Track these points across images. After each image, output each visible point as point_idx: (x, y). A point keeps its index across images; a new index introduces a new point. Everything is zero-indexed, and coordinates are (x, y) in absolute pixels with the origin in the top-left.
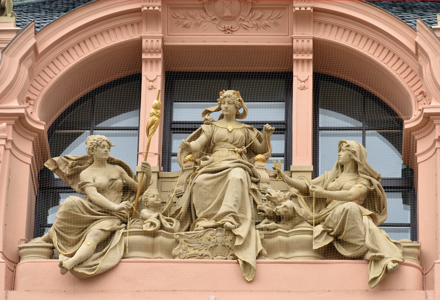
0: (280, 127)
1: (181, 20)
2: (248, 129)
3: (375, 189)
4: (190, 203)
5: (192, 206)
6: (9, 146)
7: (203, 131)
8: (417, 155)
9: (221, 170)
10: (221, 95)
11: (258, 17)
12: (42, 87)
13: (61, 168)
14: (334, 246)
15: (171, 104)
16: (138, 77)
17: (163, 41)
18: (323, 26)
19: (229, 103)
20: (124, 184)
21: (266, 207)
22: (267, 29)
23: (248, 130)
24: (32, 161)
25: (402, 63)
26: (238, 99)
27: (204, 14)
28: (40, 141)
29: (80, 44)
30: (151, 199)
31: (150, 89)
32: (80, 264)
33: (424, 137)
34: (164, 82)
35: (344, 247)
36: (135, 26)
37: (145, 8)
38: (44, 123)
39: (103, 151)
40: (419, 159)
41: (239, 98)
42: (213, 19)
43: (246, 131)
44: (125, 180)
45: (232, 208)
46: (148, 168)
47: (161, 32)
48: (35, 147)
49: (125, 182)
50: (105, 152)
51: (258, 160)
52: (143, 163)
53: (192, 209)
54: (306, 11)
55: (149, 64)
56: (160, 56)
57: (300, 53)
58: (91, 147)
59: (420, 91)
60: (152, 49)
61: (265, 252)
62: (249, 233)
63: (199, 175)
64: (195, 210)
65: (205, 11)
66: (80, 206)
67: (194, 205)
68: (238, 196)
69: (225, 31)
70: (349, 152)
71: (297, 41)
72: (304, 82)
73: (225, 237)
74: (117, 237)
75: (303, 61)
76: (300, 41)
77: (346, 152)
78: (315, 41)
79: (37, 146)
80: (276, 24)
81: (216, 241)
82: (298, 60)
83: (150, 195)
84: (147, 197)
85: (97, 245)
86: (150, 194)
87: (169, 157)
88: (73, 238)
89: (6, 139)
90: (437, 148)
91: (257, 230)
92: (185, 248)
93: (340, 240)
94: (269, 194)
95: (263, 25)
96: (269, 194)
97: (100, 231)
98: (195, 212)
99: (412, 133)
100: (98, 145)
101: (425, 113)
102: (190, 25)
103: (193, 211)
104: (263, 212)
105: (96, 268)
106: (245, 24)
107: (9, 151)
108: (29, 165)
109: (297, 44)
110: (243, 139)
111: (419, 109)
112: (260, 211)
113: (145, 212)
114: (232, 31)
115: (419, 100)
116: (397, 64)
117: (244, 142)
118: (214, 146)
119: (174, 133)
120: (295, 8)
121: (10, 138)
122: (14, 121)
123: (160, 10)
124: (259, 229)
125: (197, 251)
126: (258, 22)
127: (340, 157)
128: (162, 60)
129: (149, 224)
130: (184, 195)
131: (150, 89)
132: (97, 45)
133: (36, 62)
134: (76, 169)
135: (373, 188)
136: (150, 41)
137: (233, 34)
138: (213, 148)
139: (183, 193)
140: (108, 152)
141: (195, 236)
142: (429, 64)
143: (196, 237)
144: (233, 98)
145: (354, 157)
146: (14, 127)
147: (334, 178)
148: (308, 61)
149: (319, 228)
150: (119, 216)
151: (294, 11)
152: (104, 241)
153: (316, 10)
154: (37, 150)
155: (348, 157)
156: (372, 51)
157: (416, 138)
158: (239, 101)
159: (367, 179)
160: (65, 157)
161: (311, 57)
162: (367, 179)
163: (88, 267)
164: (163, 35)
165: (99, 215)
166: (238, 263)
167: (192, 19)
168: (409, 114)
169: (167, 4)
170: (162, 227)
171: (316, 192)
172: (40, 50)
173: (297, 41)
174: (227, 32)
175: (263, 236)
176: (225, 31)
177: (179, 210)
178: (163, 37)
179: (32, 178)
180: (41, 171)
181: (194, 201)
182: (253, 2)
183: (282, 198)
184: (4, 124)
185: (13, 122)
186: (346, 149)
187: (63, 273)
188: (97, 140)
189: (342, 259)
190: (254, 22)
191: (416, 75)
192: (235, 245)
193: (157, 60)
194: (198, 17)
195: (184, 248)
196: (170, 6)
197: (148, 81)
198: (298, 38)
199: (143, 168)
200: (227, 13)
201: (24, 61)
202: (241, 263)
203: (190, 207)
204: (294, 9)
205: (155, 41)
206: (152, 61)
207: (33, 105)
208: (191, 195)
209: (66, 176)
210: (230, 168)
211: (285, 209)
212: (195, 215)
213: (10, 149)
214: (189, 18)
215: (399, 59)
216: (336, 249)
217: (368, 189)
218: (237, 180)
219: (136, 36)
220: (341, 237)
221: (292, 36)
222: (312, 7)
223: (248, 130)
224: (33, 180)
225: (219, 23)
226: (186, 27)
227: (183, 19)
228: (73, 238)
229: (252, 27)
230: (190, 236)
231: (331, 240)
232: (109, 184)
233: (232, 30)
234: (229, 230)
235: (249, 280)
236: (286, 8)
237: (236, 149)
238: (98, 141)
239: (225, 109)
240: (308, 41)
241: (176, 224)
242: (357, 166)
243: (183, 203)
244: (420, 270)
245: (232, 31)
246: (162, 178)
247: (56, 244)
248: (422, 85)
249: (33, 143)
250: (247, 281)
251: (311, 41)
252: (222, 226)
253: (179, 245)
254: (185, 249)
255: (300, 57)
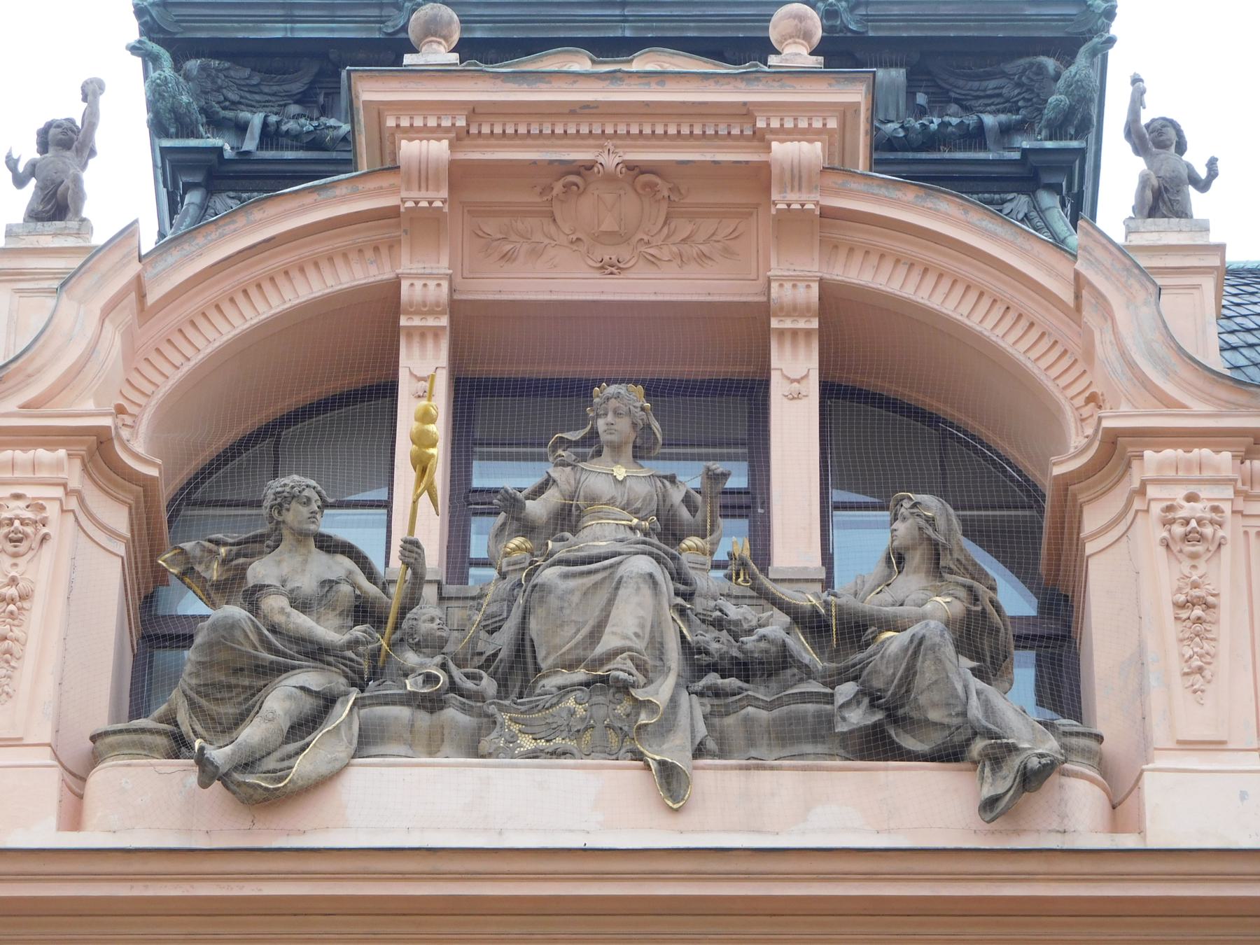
0: (736, 500)
1: (496, 243)
2: (665, 481)
3: (984, 611)
4: (523, 634)
5: (528, 643)
6: (73, 503)
7: (554, 481)
8: (1087, 538)
9: (599, 559)
10: (598, 396)
11: (685, 235)
12: (152, 388)
13: (198, 568)
14: (890, 737)
15: (465, 521)
16: (388, 390)
17: (452, 290)
18: (842, 255)
19: (617, 413)
20: (358, 597)
21: (716, 642)
22: (705, 265)
23: (663, 483)
24: (127, 548)
25: (1040, 333)
26: (638, 404)
27: (553, 229)
28: (148, 524)
29: (249, 291)
30: (424, 627)
31: (419, 397)
32: (248, 765)
33: (1101, 495)
34: (452, 396)
35: (913, 737)
36: (384, 251)
37: (410, 204)
38: (159, 461)
39: (305, 511)
40: (1090, 548)
41: (641, 403)
42: (574, 239)
43: (659, 484)
44: (359, 588)
45: (630, 639)
46: (417, 553)
47: (447, 266)
48: (140, 570)
49: (358, 592)
50: (310, 515)
51: (690, 549)
52: (405, 542)
53: (528, 648)
54: (803, 210)
55: (416, 339)
56: (444, 321)
57: (788, 315)
58: (274, 502)
59: (1087, 394)
60: (425, 305)
61: (711, 745)
62: (673, 702)
63: (544, 569)
64: (534, 652)
65: (554, 220)
66: (251, 630)
67: (532, 641)
68: (642, 613)
69: (602, 268)
70: (919, 520)
71: (781, 285)
72: (798, 381)
73: (612, 706)
74: (342, 712)
75: (795, 333)
76: (788, 285)
77: (910, 521)
78: (822, 283)
79: (144, 568)
80: (728, 252)
81: (591, 717)
82: (781, 333)
83: (423, 618)
84: (414, 622)
85: (292, 727)
86: (424, 614)
87: (463, 568)
88: (228, 710)
89: (65, 485)
90: (1137, 512)
91: (694, 696)
92: (512, 737)
93: (904, 719)
94: (721, 610)
95: (695, 255)
96: (721, 610)
97: (298, 692)
98: (535, 658)
99: (1070, 488)
100: (294, 497)
101: (1107, 430)
102: (515, 254)
103: (529, 654)
104: (707, 653)
105: (288, 775)
106: (652, 253)
107: (71, 516)
108: (120, 560)
109: (781, 293)
110: (651, 500)
111: (1085, 435)
112: (700, 653)
113: (411, 658)
114: (619, 268)
115: (1084, 416)
116: (1026, 338)
117: (655, 507)
118: (579, 517)
119: (475, 514)
120: (776, 205)
121: (74, 483)
122: (85, 448)
123: (446, 210)
124: (701, 694)
125: (542, 743)
126: (686, 248)
127: (895, 533)
128: (448, 328)
129: (420, 679)
130: (506, 626)
131: (419, 397)
132: (288, 294)
133: (140, 328)
134: (238, 565)
135: (979, 608)
136: (418, 284)
137: (621, 276)
138: (578, 521)
139: (503, 620)
140: (318, 516)
141: (538, 706)
142: (1109, 322)
143: (540, 707)
144: (626, 401)
145: (930, 531)
146: (85, 468)
147: (879, 586)
148: (808, 333)
149: (847, 690)
150: (347, 670)
151: (773, 211)
152: (307, 721)
153: (827, 214)
154: (143, 578)
155: (916, 532)
156: (965, 308)
157: (1082, 498)
158: (643, 409)
159: (964, 586)
160: (210, 541)
161: (815, 324)
162: (964, 586)
163: (269, 772)
164: (451, 271)
165: (292, 658)
166: (648, 767)
167: (522, 240)
168: (1058, 441)
169: (461, 202)
170: (453, 687)
171: (839, 607)
172: (151, 299)
173: (781, 285)
174: (606, 271)
175: (708, 709)
176: (602, 268)
177: (495, 655)
178: (451, 276)
179: (126, 590)
180: (146, 597)
181: (534, 626)
182: (672, 198)
183: (754, 623)
184: (62, 453)
185: (82, 450)
186: (912, 513)
187: (204, 784)
188: (291, 484)
189: (909, 760)
190: (674, 249)
191: (1076, 361)
192: (639, 723)
193: (436, 332)
194: (538, 237)
195: (507, 737)
196: (468, 208)
197: (414, 381)
198: (782, 280)
199: (407, 554)
200: (608, 224)
201: (111, 315)
202: (653, 765)
203: (523, 647)
204: (772, 206)
205: (432, 284)
206: (423, 333)
207: (132, 427)
208: (524, 618)
209: (212, 585)
210: (620, 554)
211: (763, 645)
212: (535, 663)
213: (73, 511)
214: (513, 237)
215: (1032, 324)
216: (897, 743)
217: (969, 611)
218: (641, 576)
219: (387, 274)
220: (901, 712)
221: (769, 273)
222: (817, 203)
223: (663, 483)
224: (127, 595)
225: (588, 249)
226: (506, 258)
227: (499, 239)
228: (228, 710)
229: (669, 260)
230: (523, 708)
231: (879, 716)
232: (320, 594)
233: (621, 265)
234: (624, 688)
235: (676, 806)
236: (751, 214)
237: (635, 521)
238: (293, 487)
239: (606, 428)
240: (808, 287)
241: (488, 684)
242: (939, 554)
243: (503, 640)
244: (1104, 790)
245: (619, 268)
246: (450, 599)
247: (185, 728)
248: (1091, 382)
249: (130, 509)
250: (671, 808)
251: (815, 288)
252: (604, 680)
253: (496, 730)
254: (512, 740)
255: (788, 324)
